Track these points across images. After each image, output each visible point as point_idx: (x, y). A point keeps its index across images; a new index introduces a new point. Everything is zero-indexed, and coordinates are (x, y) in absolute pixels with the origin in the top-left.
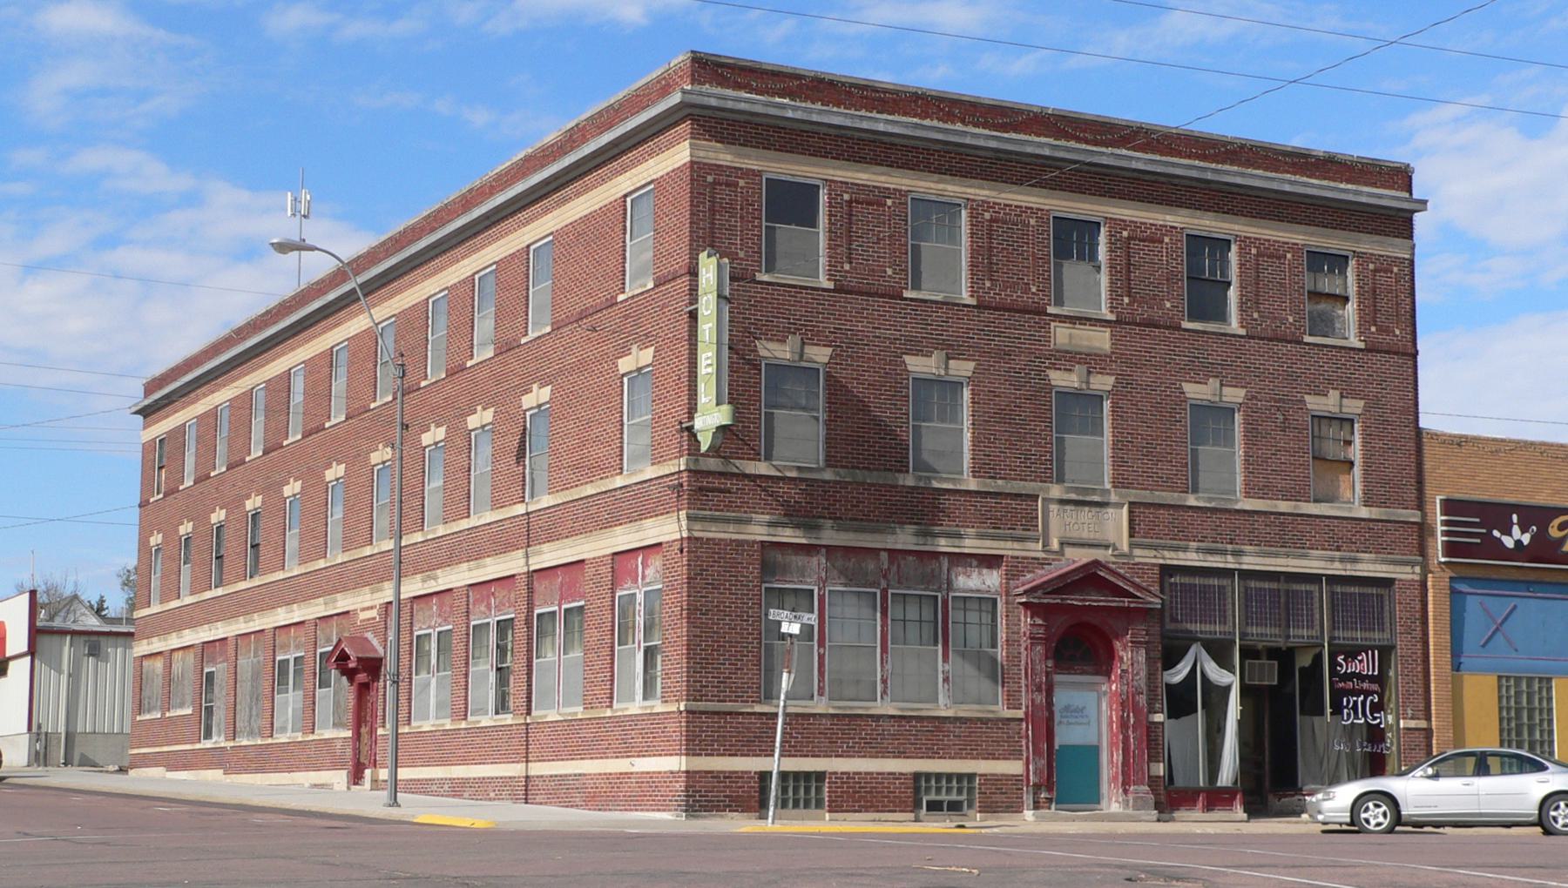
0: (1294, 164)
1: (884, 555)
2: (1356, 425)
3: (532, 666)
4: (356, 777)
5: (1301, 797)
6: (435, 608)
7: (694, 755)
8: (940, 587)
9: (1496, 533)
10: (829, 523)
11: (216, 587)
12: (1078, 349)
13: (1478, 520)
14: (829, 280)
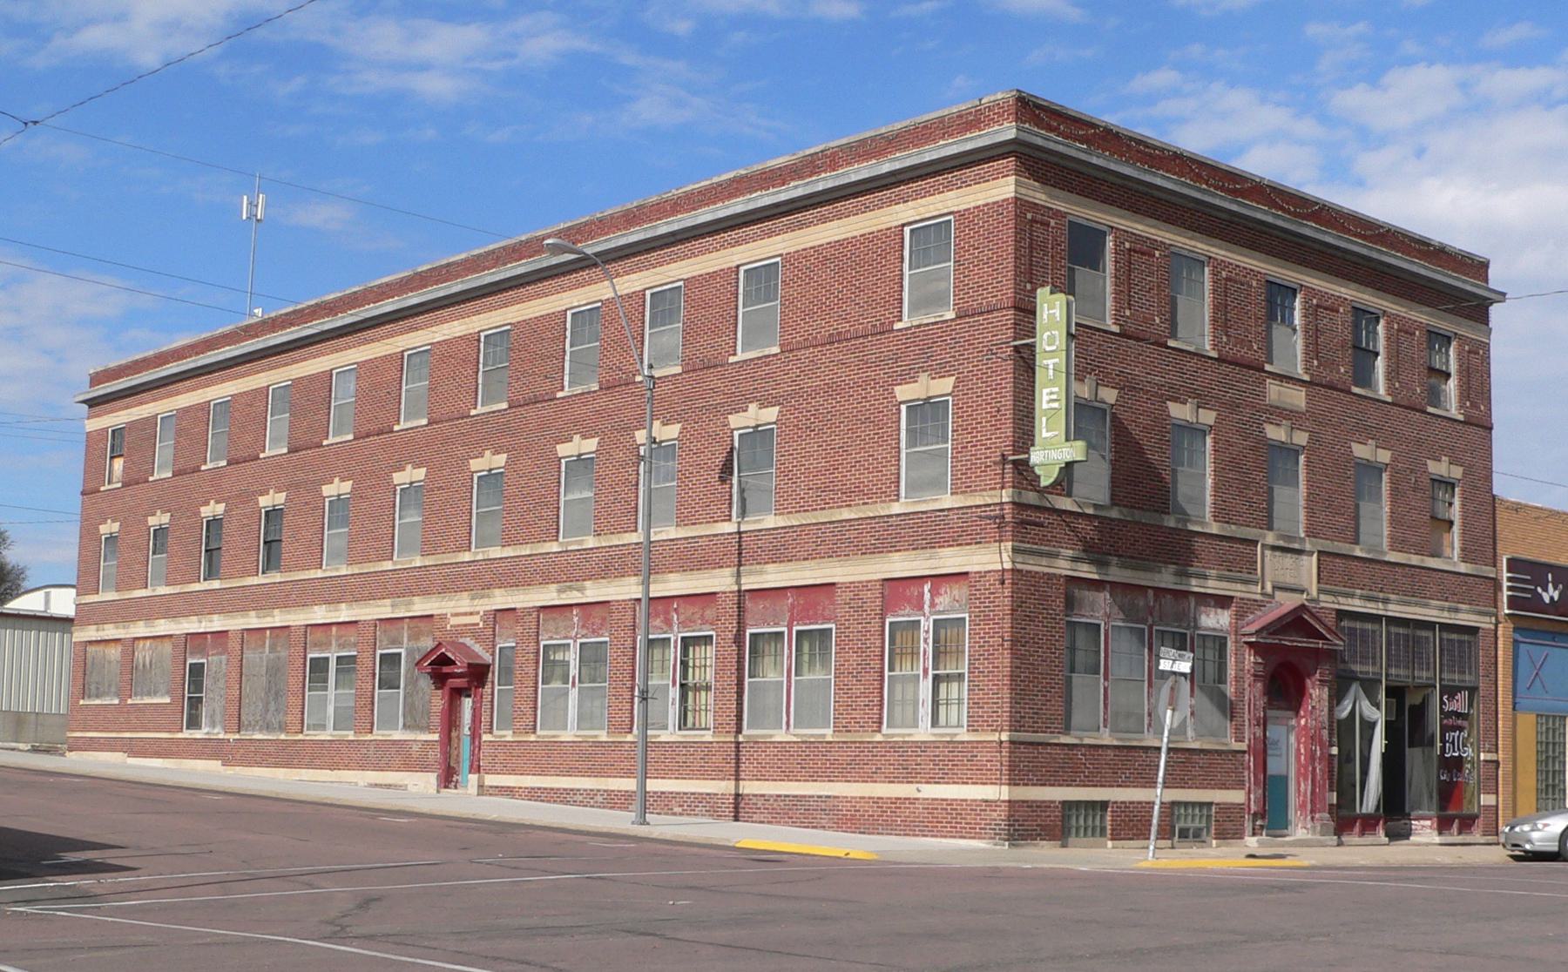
0: (1419, 251)
1: (1151, 592)
2: (1457, 489)
3: (743, 684)
4: (448, 777)
5: (1407, 822)
6: (576, 619)
7: (1015, 785)
8: (1189, 625)
9: (1539, 590)
10: (1115, 560)
11: (205, 579)
12: (1283, 406)
13: (1529, 578)
14: (1115, 323)
